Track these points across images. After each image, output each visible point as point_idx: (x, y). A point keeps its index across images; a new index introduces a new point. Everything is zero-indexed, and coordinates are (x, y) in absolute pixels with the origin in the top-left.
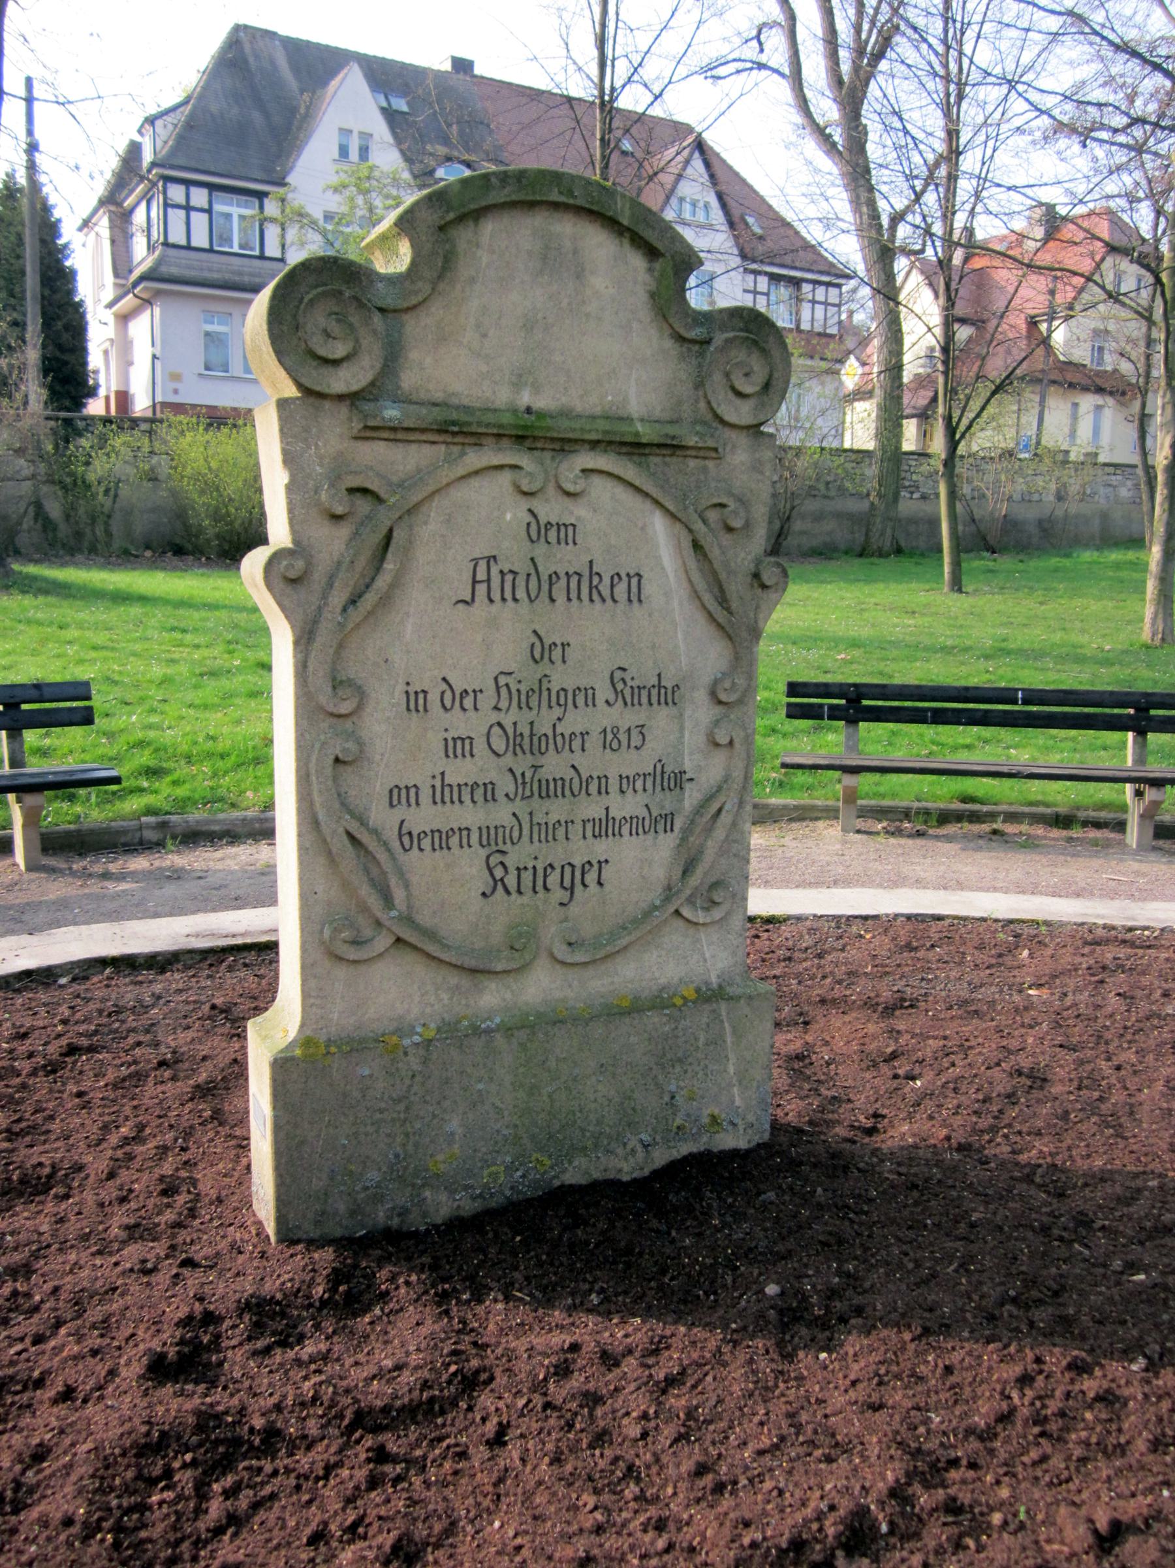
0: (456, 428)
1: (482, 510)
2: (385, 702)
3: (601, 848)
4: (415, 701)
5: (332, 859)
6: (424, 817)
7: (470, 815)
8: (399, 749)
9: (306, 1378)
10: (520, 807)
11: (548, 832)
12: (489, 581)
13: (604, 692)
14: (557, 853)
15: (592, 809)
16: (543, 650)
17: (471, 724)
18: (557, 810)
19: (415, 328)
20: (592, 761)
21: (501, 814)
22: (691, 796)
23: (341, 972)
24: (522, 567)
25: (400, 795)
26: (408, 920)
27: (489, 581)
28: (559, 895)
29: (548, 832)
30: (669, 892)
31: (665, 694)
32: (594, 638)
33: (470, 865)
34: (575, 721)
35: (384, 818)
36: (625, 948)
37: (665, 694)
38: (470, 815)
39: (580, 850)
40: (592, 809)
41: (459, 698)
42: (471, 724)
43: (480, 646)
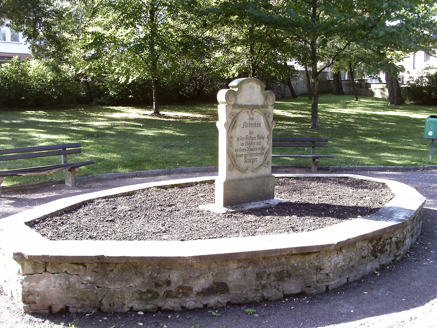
0: (242, 107)
1: (244, 117)
2: (235, 139)
3: (256, 157)
4: (238, 139)
5: (230, 158)
6: (239, 153)
7: (243, 153)
8: (236, 145)
9: (111, 77)
10: (248, 152)
11: (252, 155)
12: (245, 125)
13: (257, 138)
14: (252, 158)
15: (255, 152)
16: (251, 133)
17: (243, 142)
18: (252, 152)
19: (239, 96)
20: (256, 146)
21: (246, 153)
22: (265, 151)
23: (230, 172)
24: (249, 123)
25: (236, 150)
26: (237, 166)
27: (245, 125)
28: (252, 163)
29: (252, 155)
30: (263, 163)
31: (263, 138)
32: (256, 131)
33: (243, 159)
34: (254, 141)
35: (235, 153)
36: (46, 141)
37: (263, 138)
38: (243, 153)
39: (255, 157)
40: (255, 152)
41: (242, 139)
42: (243, 142)
43: (246, 132)
